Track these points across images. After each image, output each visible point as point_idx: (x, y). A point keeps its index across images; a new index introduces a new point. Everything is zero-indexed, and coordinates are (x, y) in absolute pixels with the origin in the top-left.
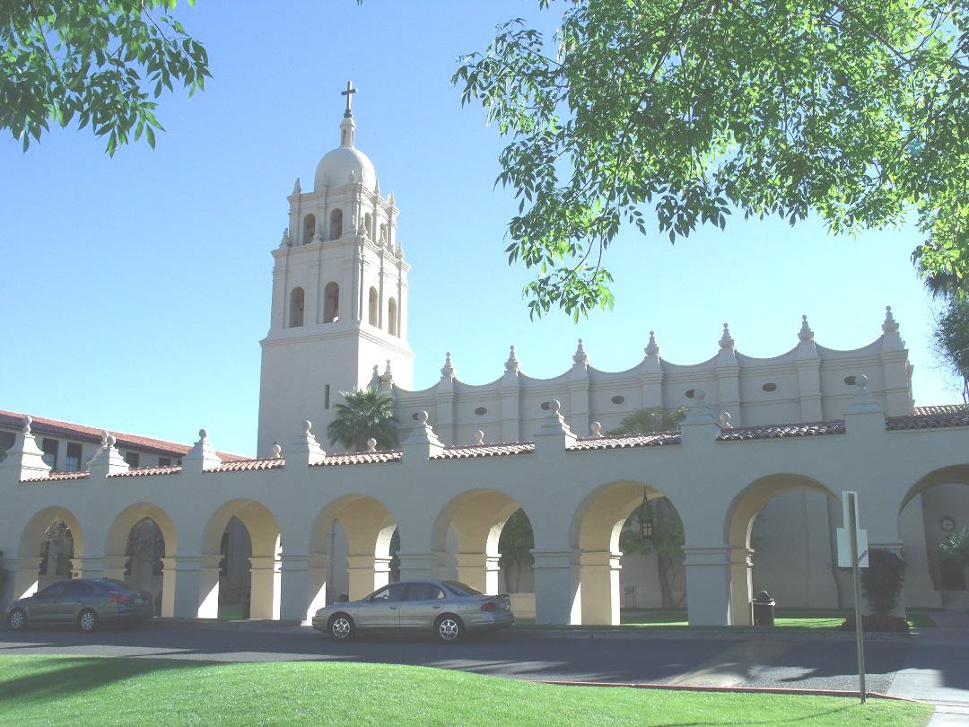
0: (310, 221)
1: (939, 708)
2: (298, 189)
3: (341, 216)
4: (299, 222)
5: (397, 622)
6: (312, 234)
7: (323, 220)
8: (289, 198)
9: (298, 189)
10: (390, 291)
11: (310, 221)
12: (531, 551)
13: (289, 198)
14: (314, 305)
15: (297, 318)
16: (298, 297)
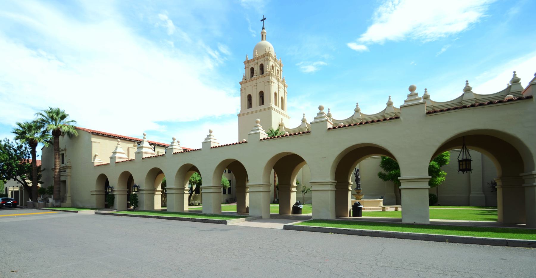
1: (314, 188)
5: (383, 227)
10: (281, 94)
11: (252, 70)
12: (399, 178)
14: (255, 99)
15: (250, 105)
16: (250, 97)
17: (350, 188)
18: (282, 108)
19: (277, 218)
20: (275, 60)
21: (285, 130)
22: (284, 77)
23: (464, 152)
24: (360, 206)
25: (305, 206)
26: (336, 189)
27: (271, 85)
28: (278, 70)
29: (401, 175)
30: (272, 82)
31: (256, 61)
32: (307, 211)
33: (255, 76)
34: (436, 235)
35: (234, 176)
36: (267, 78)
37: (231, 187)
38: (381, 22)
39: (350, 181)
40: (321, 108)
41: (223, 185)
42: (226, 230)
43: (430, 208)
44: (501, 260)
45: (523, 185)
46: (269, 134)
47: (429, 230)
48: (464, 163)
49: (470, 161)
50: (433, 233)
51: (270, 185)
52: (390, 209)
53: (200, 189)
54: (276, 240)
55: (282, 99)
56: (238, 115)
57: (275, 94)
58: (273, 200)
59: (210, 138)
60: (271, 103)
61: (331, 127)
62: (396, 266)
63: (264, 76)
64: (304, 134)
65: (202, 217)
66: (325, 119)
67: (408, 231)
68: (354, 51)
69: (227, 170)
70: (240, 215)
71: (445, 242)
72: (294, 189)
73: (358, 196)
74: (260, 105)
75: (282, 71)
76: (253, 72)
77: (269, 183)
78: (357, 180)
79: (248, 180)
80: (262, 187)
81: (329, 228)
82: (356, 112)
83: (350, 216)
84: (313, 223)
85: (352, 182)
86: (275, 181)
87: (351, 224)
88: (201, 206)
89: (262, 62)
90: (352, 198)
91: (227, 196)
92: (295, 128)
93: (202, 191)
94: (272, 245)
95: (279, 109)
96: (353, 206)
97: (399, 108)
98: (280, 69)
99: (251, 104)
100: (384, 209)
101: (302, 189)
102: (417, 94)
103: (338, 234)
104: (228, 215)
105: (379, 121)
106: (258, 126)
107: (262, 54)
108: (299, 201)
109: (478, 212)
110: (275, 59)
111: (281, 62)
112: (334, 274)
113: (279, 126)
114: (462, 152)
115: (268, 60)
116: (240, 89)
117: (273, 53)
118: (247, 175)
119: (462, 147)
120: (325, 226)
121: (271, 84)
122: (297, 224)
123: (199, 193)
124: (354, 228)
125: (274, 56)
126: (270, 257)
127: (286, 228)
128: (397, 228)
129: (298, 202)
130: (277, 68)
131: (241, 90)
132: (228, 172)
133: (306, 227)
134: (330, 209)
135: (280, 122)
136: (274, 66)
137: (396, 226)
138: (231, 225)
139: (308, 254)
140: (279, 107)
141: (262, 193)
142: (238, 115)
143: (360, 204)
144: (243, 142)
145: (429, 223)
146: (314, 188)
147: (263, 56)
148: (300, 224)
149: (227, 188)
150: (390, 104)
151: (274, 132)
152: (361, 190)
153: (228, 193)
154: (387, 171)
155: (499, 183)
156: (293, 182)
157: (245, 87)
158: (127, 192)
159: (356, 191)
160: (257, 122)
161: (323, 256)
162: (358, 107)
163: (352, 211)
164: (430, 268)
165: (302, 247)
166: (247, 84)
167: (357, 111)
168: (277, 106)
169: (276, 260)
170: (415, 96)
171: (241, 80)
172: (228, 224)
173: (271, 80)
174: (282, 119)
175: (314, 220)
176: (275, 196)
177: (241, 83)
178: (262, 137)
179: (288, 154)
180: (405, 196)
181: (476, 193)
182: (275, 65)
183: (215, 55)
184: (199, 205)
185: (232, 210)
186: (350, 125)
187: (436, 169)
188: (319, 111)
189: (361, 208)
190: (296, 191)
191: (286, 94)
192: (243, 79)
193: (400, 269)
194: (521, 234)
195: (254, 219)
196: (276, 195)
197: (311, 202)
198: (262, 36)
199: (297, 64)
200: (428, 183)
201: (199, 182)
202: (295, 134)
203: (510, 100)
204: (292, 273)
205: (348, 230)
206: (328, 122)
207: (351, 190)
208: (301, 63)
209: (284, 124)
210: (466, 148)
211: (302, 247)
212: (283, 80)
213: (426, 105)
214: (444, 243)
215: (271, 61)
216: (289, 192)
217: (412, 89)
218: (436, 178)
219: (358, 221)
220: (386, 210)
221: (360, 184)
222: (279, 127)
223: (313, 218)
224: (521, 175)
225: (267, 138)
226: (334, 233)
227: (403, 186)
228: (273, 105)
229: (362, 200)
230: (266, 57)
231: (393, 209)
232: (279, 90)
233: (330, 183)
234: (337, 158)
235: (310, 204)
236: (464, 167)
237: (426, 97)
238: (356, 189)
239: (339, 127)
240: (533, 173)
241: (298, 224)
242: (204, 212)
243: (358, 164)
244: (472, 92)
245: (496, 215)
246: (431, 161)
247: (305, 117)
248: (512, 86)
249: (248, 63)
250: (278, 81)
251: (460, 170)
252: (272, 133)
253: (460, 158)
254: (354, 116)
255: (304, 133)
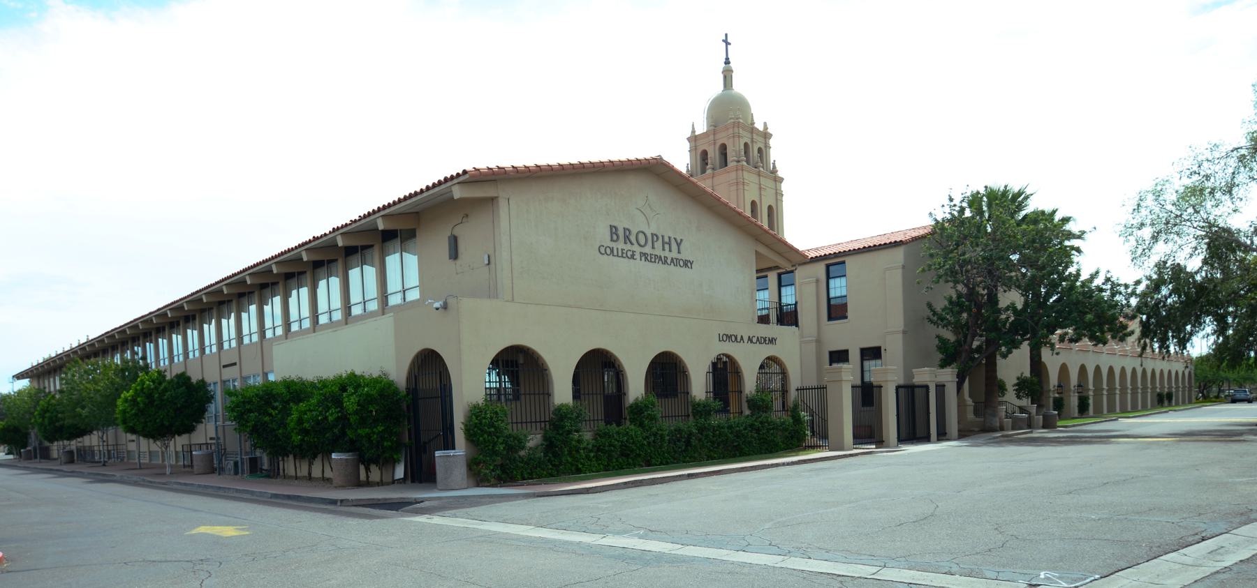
0: (705, 154)
2: (693, 131)
3: (726, 149)
4: (715, 150)
6: (707, 164)
7: (713, 154)
8: (688, 139)
9: (693, 131)
13: (688, 139)
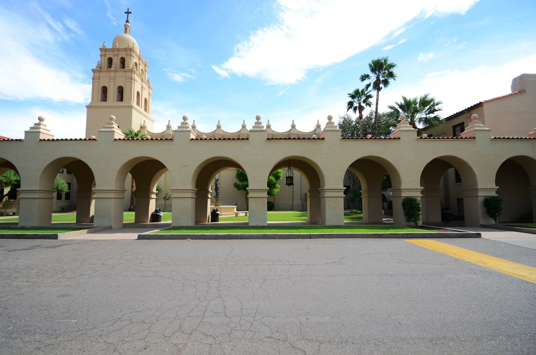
1: (175, 195)
10: (145, 95)
14: (112, 93)
17: (209, 196)
18: (146, 110)
19: (131, 228)
20: (140, 58)
21: (172, 132)
22: (149, 79)
23: (290, 172)
24: (218, 213)
25: (165, 213)
26: (196, 197)
27: (133, 83)
28: (142, 70)
29: (249, 187)
30: (134, 79)
31: (116, 52)
32: (166, 218)
33: (114, 68)
34: (270, 234)
35: (76, 180)
36: (128, 74)
37: (70, 192)
38: (239, 57)
39: (210, 190)
40: (185, 118)
41: (58, 188)
42: (55, 247)
43: (268, 213)
44: (307, 249)
45: (320, 196)
46: (126, 135)
47: (266, 230)
48: (289, 179)
49: (292, 178)
50: (269, 233)
51: (125, 191)
52: (242, 214)
53: (18, 193)
54: (126, 253)
55: (146, 100)
56: (88, 107)
57: (138, 93)
58: (129, 207)
59: (40, 128)
60: (132, 102)
61: (194, 138)
62: (252, 263)
63: (125, 71)
64: (166, 141)
65: (16, 231)
66: (188, 129)
67: (252, 232)
68: (217, 75)
69: (65, 171)
70: (79, 227)
71: (276, 239)
72: (154, 196)
73: (217, 203)
74: (118, 101)
75: (147, 71)
76: (112, 63)
77: (124, 189)
78: (217, 189)
79: (95, 185)
80: (113, 193)
81: (187, 235)
82: (218, 128)
83: (208, 222)
84: (172, 231)
85: (211, 190)
86: (132, 186)
87: (208, 230)
88: (17, 217)
89: (124, 56)
90: (211, 205)
91: (63, 202)
92: (274, 130)
93: (19, 196)
94: (120, 259)
95: (142, 110)
96: (212, 213)
97: (249, 130)
98: (145, 69)
99: (106, 97)
100: (237, 215)
101: (163, 196)
102: (334, 123)
103: (195, 240)
104: (62, 227)
105: (234, 139)
106: (112, 124)
107: (124, 48)
108: (158, 208)
109: (299, 215)
110: (140, 57)
111: (146, 62)
112: (187, 280)
113: (141, 128)
114: (288, 171)
115: (131, 55)
116: (92, 77)
117: (137, 49)
118: (93, 178)
119: (288, 167)
120: (184, 233)
121: (133, 82)
122: (154, 233)
123: (15, 198)
124: (210, 233)
125: (138, 54)
126: (116, 273)
127: (140, 238)
128: (244, 230)
129: (158, 209)
130: (142, 67)
131: (93, 79)
132: (67, 173)
133: (164, 235)
134: (190, 216)
135: (143, 124)
136: (138, 63)
137: (244, 229)
138: (65, 240)
139: (163, 263)
140: (141, 108)
141: (113, 199)
142: (88, 107)
143: (217, 210)
144: (90, 139)
145: (267, 225)
146: (175, 195)
147: (126, 50)
148: (157, 232)
149: (64, 193)
150: (244, 127)
151: (134, 133)
152: (219, 198)
153: (66, 199)
154: (240, 182)
155: (308, 195)
156: (153, 188)
157: (99, 76)
158: (343, 193)
159: (215, 199)
160: (111, 119)
161: (178, 263)
162: (220, 124)
163: (210, 216)
164: (264, 261)
165: (156, 257)
166: (102, 74)
167: (219, 127)
168: (139, 106)
169: (123, 276)
170: (111, 124)
171: (94, 67)
172: (59, 238)
173: (133, 78)
174: (144, 121)
175: (173, 227)
176: (132, 203)
177: (93, 71)
178: (117, 137)
179: (149, 159)
180: (252, 204)
181: (297, 202)
182: (139, 64)
183: (58, 27)
184: (14, 214)
185: (69, 220)
186: (162, 139)
187: (273, 183)
188: (183, 121)
189: (218, 214)
190: (156, 197)
191: (150, 96)
192: (97, 67)
193: (243, 265)
194: (318, 230)
195: (100, 230)
196: (133, 201)
197: (171, 209)
198: (125, 29)
199: (164, 69)
200: (343, 192)
201: (15, 183)
202: (157, 139)
203: (314, 139)
204: (142, 287)
205: (204, 235)
206: (191, 133)
207: (210, 198)
208: (168, 69)
209: (147, 126)
210: (290, 168)
211: (156, 257)
212: (148, 81)
213: (266, 132)
214: (275, 240)
215: (135, 58)
216: (148, 198)
217: (258, 118)
218: (273, 189)
219: (215, 226)
220: (239, 215)
221: (219, 193)
222: (140, 129)
223: (173, 225)
224: (319, 189)
225: (124, 139)
226: (192, 239)
227: (250, 195)
228: (134, 104)
229: (220, 206)
230: (129, 52)
231: (244, 214)
232: (142, 90)
233: (191, 191)
234: (198, 167)
235: (170, 211)
236: (289, 183)
237: (269, 127)
238: (215, 196)
239: (201, 139)
240: (325, 188)
241: (156, 233)
242: (20, 225)
243: (218, 174)
244: (296, 128)
245: (306, 216)
246: (270, 175)
247: (170, 124)
248: (317, 129)
249: (105, 51)
250: (142, 80)
251: (287, 184)
252: (132, 134)
253: (287, 176)
254: (165, 132)
255: (166, 139)
